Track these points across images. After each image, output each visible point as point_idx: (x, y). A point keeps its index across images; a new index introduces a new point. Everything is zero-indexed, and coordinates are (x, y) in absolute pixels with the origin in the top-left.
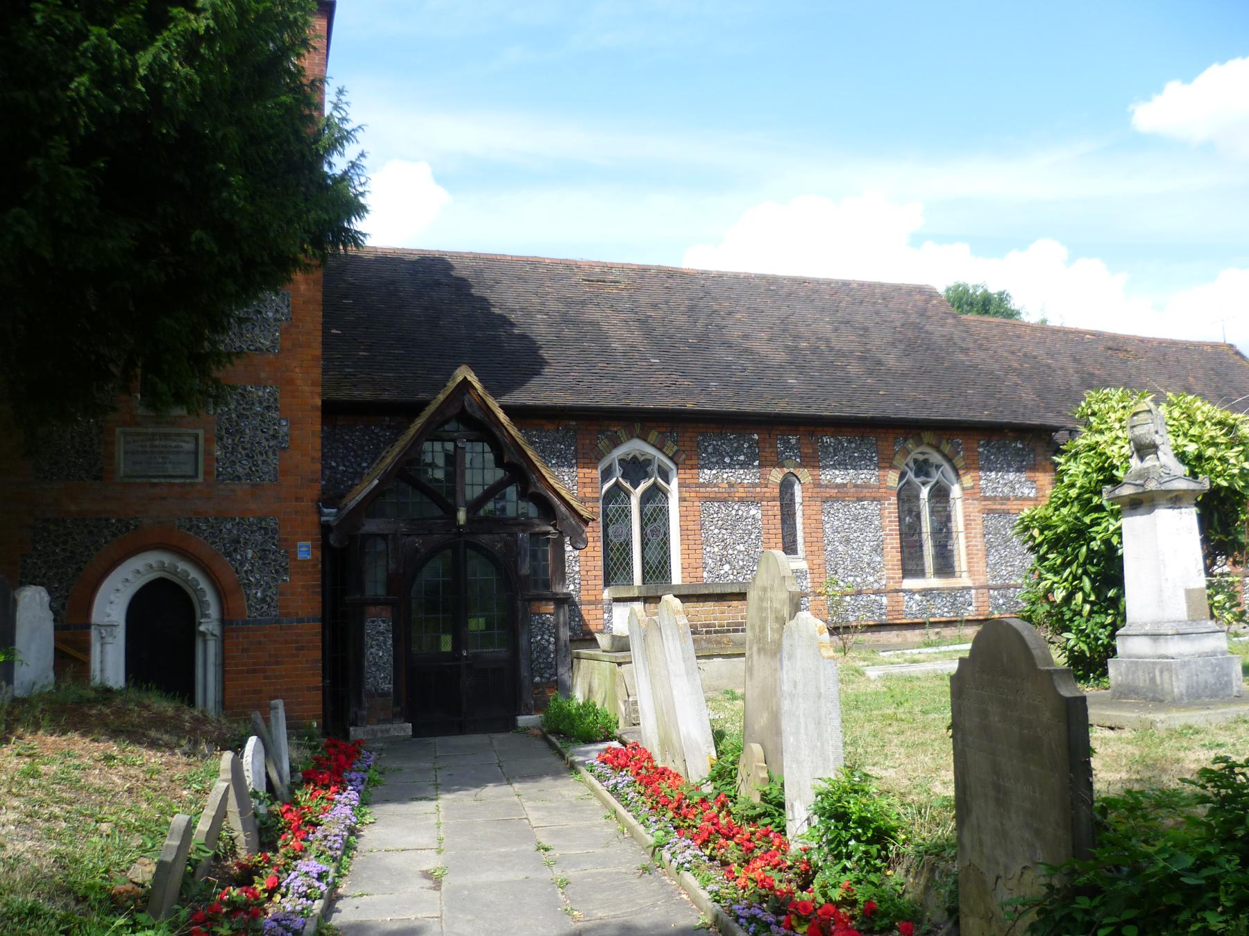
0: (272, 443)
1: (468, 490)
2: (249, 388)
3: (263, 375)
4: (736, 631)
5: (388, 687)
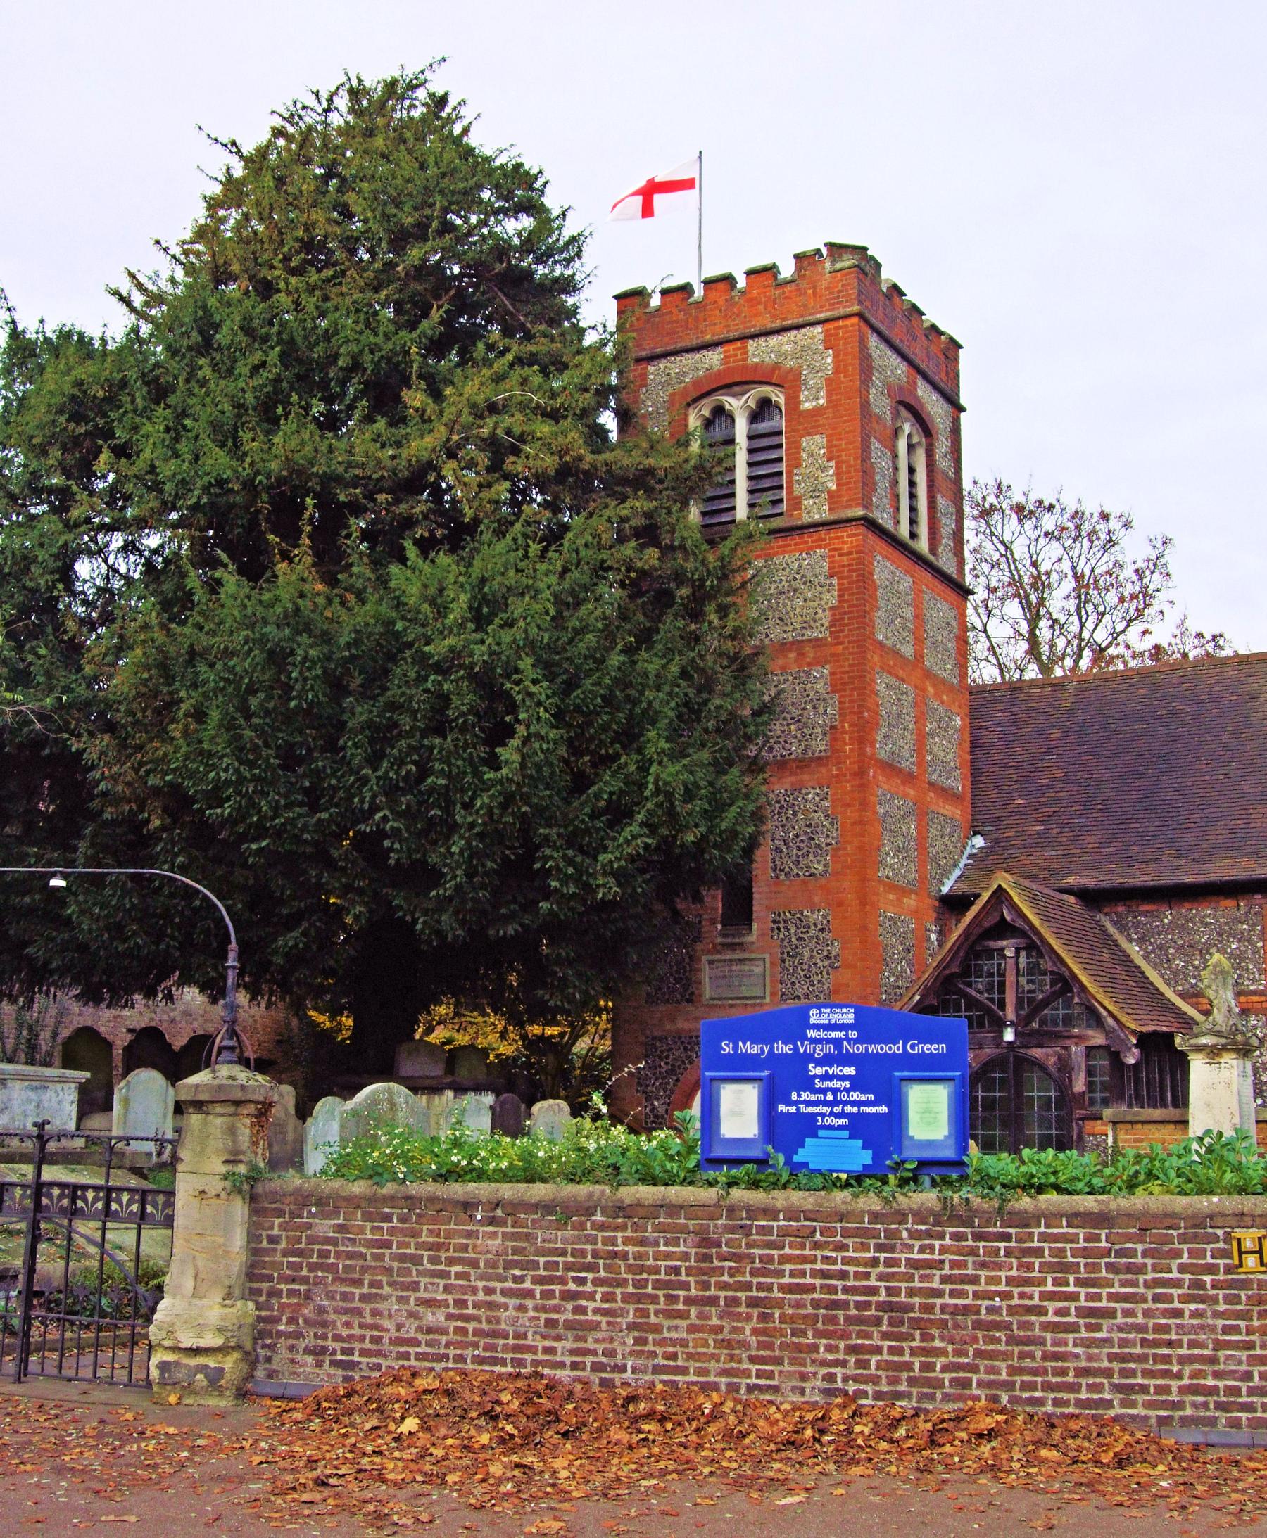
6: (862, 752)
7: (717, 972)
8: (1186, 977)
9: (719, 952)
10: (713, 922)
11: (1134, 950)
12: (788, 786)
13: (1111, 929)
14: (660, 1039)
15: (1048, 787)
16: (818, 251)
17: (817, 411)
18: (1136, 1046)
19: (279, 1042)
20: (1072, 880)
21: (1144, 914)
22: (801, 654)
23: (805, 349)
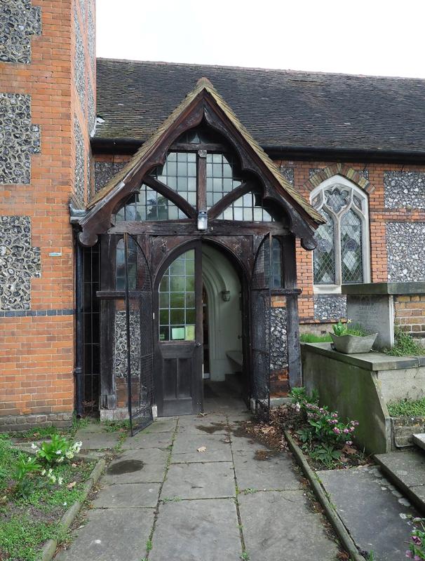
0: (25, 148)
1: (209, 195)
3: (15, 84)
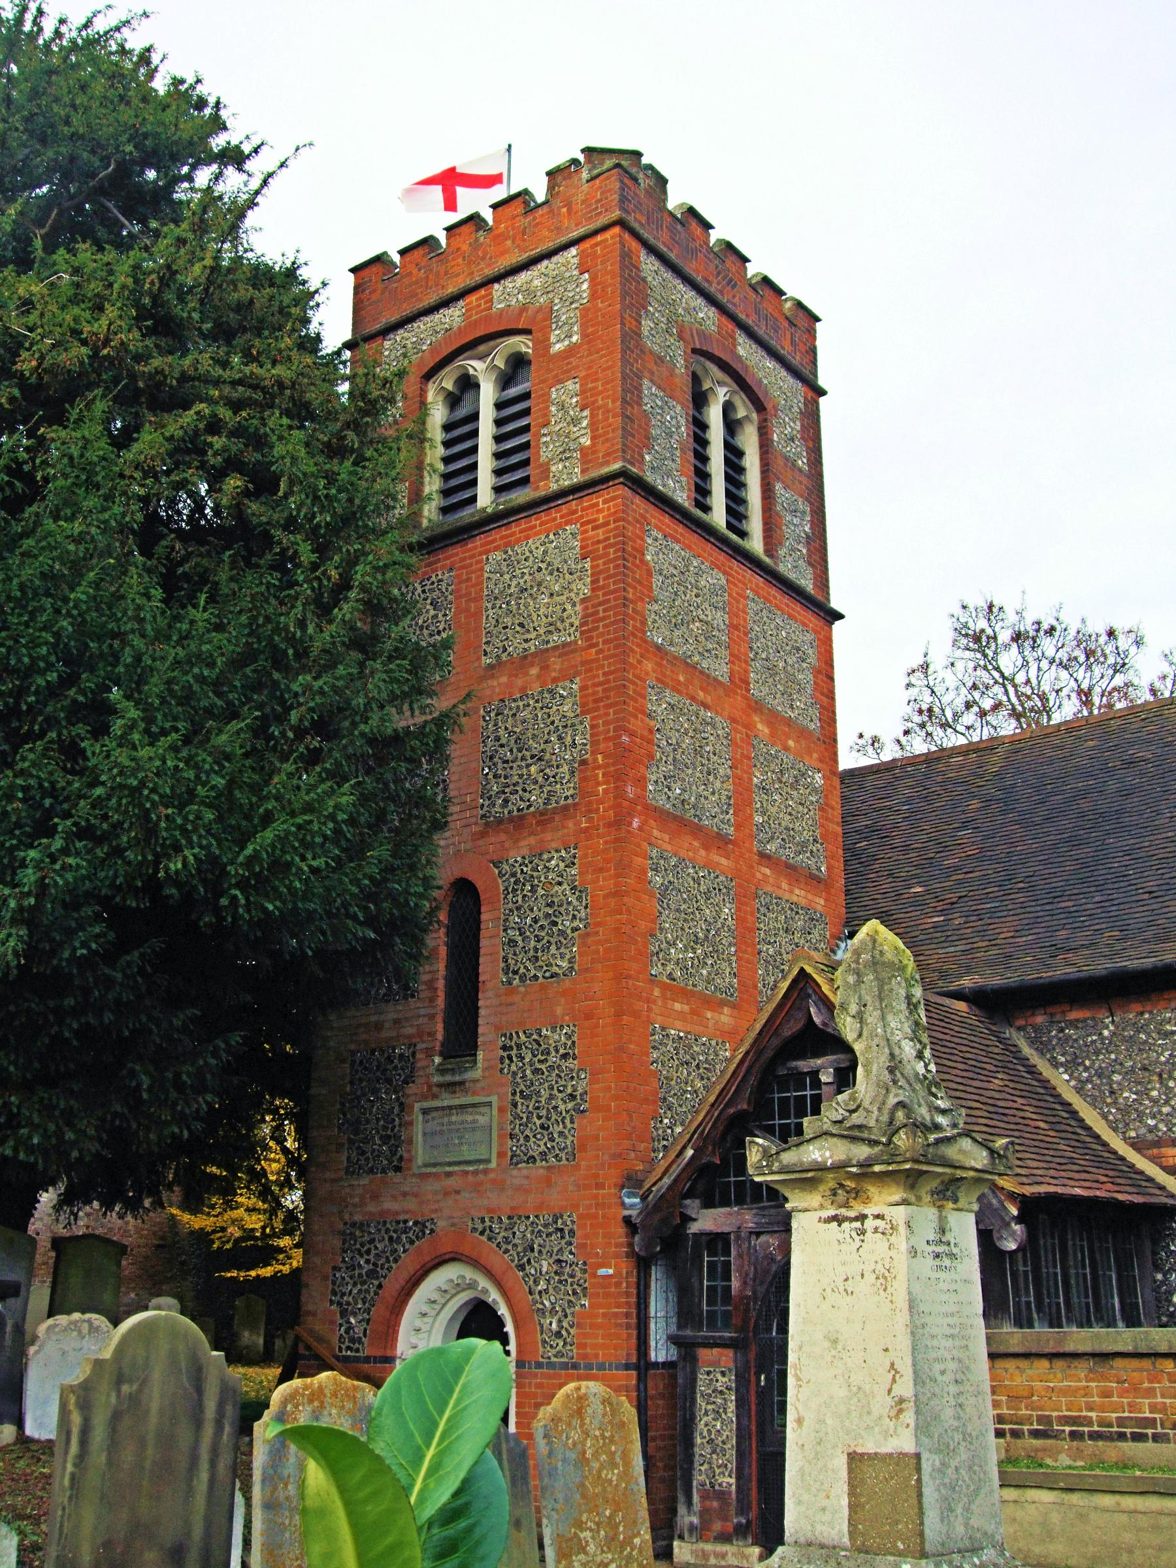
0: (570, 1105)
2: (544, 1032)
4: (1138, 1438)
5: (728, 1481)
6: (619, 793)
7: (433, 1126)
8: (1141, 1116)
9: (435, 1097)
10: (429, 1053)
11: (1061, 1080)
12: (525, 851)
13: (1027, 1050)
14: (362, 1226)
15: (957, 868)
16: (575, 162)
17: (571, 351)
18: (1019, 1219)
19: (158, 1246)
20: (967, 982)
21: (1073, 1024)
22: (545, 668)
23: (557, 279)
